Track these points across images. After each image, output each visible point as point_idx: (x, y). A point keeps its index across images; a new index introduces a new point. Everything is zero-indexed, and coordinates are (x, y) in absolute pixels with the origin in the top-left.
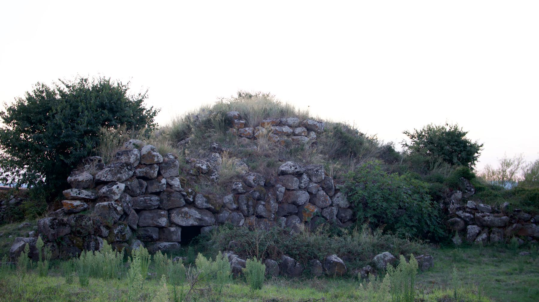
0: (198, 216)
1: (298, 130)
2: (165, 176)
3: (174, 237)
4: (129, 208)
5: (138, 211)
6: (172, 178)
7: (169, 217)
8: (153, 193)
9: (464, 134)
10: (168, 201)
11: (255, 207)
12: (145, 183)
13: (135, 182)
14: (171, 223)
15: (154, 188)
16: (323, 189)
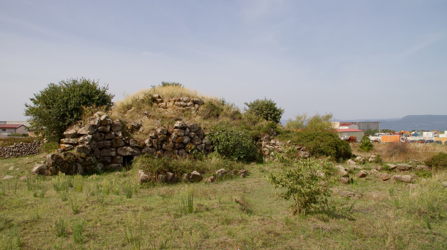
0: (132, 150)
1: (189, 104)
2: (114, 130)
3: (119, 161)
4: (94, 148)
5: (100, 149)
6: (118, 131)
7: (116, 151)
8: (107, 140)
9: (275, 104)
10: (116, 143)
11: (162, 145)
12: (103, 135)
13: (98, 134)
14: (117, 154)
15: (107, 137)
16: (197, 135)
